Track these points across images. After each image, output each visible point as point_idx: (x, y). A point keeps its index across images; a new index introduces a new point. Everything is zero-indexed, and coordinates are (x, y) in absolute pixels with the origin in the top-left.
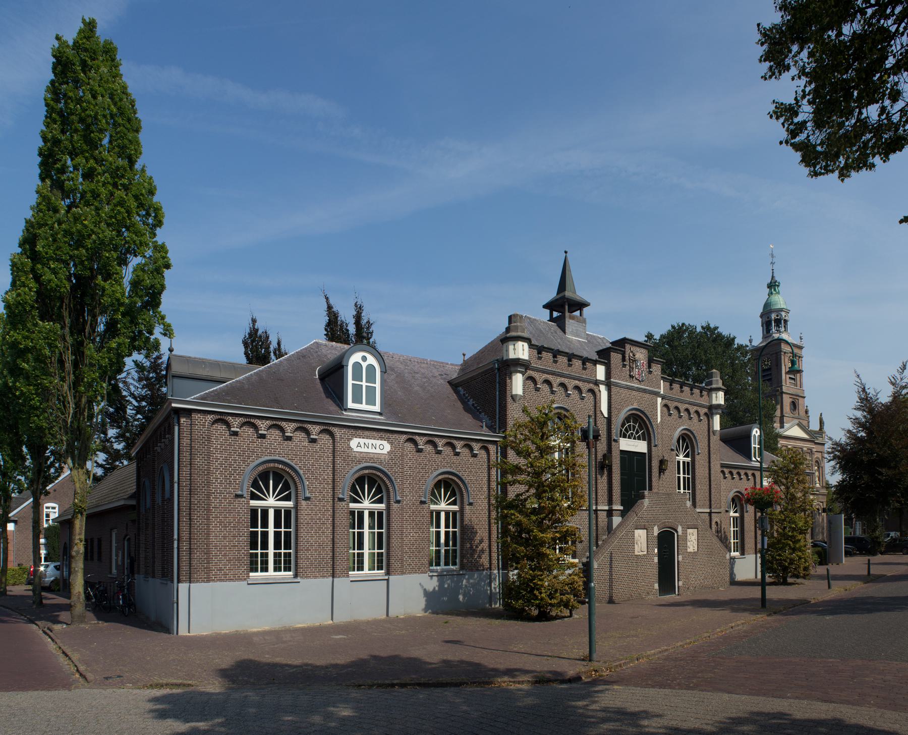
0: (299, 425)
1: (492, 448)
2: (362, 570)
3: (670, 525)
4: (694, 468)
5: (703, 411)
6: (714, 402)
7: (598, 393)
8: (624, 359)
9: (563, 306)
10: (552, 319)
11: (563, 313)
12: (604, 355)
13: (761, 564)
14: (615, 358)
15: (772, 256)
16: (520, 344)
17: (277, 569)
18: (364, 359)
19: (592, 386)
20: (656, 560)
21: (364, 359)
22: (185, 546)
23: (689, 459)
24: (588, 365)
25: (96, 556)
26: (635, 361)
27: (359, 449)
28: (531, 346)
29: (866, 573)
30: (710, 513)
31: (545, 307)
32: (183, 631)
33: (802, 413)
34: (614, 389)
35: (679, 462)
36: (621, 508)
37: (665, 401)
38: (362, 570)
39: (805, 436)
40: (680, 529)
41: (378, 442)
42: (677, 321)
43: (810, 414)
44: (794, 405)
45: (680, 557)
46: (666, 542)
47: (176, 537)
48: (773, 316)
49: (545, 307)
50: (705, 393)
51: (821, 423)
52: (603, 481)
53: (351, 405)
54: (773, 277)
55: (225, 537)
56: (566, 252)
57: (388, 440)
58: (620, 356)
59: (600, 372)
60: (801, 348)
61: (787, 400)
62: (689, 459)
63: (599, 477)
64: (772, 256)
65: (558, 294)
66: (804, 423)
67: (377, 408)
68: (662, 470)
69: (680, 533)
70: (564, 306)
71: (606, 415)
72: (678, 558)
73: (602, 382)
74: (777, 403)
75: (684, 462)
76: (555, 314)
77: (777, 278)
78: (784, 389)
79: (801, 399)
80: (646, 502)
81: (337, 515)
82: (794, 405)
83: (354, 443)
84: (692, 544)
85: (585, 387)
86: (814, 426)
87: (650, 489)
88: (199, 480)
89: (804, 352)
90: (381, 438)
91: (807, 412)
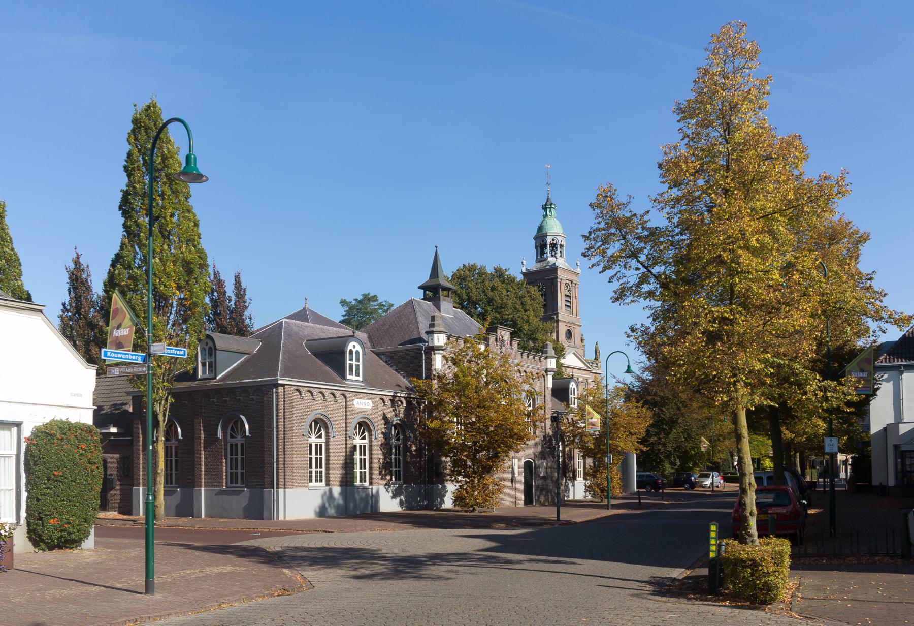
6: (549, 367)
8: (496, 341)
13: (28, 483)
17: (316, 481)
18: (354, 346)
20: (523, 480)
21: (354, 346)
22: (281, 466)
26: (503, 341)
29: (562, 509)
31: (419, 287)
32: (281, 518)
33: (578, 341)
39: (584, 367)
42: (469, 261)
43: (585, 342)
49: (419, 287)
53: (349, 377)
57: (371, 399)
61: (563, 329)
65: (430, 278)
66: (581, 352)
67: (360, 378)
78: (560, 317)
79: (576, 328)
82: (569, 334)
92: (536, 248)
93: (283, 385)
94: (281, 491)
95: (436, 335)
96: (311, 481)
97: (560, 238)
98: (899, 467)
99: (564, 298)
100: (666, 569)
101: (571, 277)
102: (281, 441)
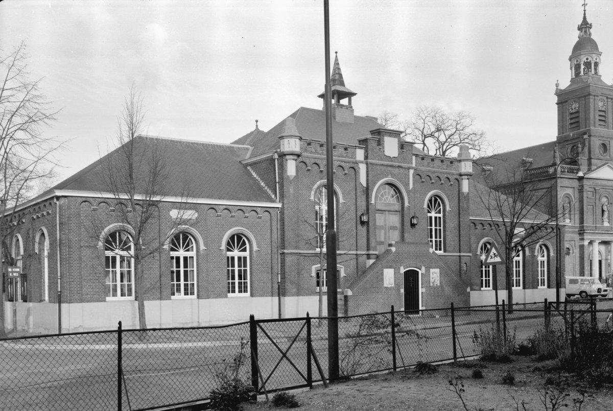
35: (431, 218)
38: (235, 292)
54: (585, 18)
77: (589, 21)
92: (571, 68)
95: (286, 140)
96: (234, 291)
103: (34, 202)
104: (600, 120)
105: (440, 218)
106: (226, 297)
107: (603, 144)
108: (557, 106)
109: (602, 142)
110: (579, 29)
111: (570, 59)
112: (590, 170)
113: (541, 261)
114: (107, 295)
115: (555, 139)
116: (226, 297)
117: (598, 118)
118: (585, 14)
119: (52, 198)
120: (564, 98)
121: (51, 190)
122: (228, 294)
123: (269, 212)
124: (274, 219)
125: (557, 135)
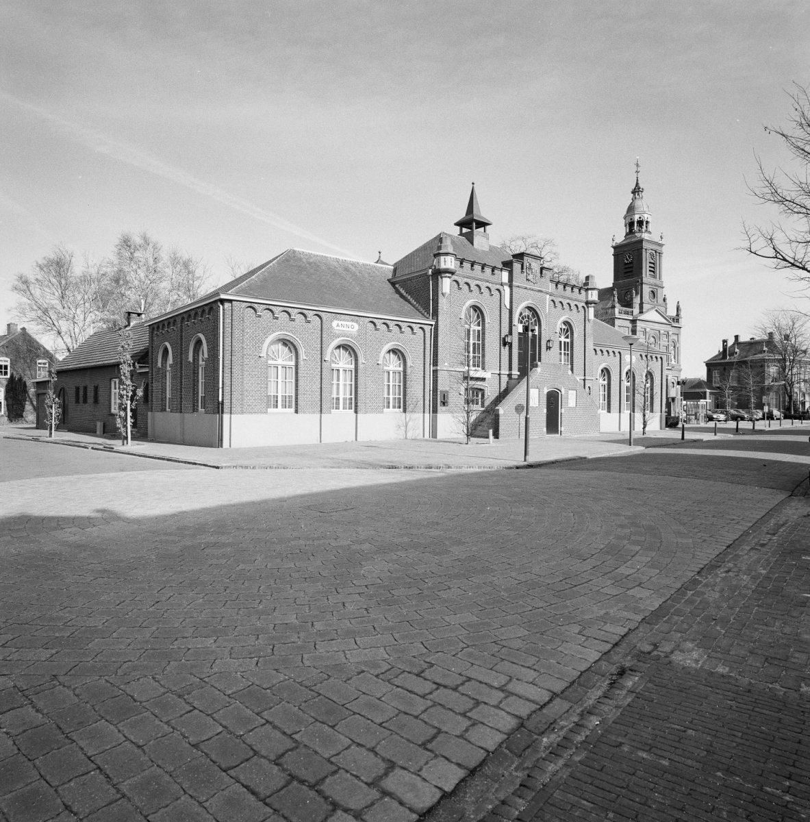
0: (249, 304)
1: (427, 329)
2: (339, 409)
3: (556, 387)
4: (572, 347)
5: (580, 305)
6: (590, 299)
7: (502, 292)
8: (522, 268)
9: (471, 224)
10: (461, 234)
11: (471, 228)
12: (508, 265)
14: (517, 266)
15: (637, 165)
16: (449, 258)
17: (394, 407)
19: (499, 287)
23: (568, 340)
24: (496, 271)
25: (81, 399)
27: (338, 328)
28: (457, 259)
30: (584, 380)
31: (457, 224)
33: (660, 300)
34: (514, 289)
35: (561, 342)
36: (519, 373)
37: (553, 298)
38: (339, 409)
39: (665, 321)
40: (563, 390)
41: (350, 323)
43: (667, 301)
44: (653, 294)
45: (563, 410)
46: (553, 401)
47: (221, 386)
48: (636, 218)
49: (457, 224)
50: (582, 291)
51: (678, 309)
52: (505, 351)
54: (637, 184)
55: (252, 384)
56: (473, 184)
57: (357, 322)
58: (520, 266)
59: (505, 276)
60: (661, 245)
61: (646, 290)
62: (568, 340)
63: (502, 348)
64: (637, 165)
66: (663, 309)
68: (548, 348)
69: (563, 393)
70: (471, 223)
71: (508, 307)
72: (562, 411)
73: (506, 284)
74: (637, 294)
75: (565, 342)
76: (465, 230)
77: (641, 185)
78: (645, 280)
80: (539, 369)
81: (323, 371)
82: (653, 294)
83: (335, 323)
84: (572, 403)
85: (493, 287)
86: (672, 312)
87: (540, 360)
88: (237, 346)
89: (664, 249)
90: (352, 321)
91: (664, 300)
92: (626, 226)
93: (230, 301)
94: (226, 417)
95: (442, 258)
96: (338, 408)
97: (646, 216)
98: (664, 414)
99: (648, 265)
100: (763, 458)
101: (655, 247)
102: (227, 362)
103: (171, 315)
104: (650, 271)
105: (568, 343)
106: (382, 412)
107: (652, 291)
108: (613, 257)
109: (651, 289)
110: (632, 193)
111: (625, 218)
112: (641, 312)
113: (85, 401)
114: (268, 406)
115: (611, 285)
116: (382, 412)
117: (648, 269)
118: (637, 180)
119: (216, 301)
120: (619, 251)
121: (216, 293)
122: (332, 410)
123: (424, 332)
124: (428, 335)
125: (613, 282)
